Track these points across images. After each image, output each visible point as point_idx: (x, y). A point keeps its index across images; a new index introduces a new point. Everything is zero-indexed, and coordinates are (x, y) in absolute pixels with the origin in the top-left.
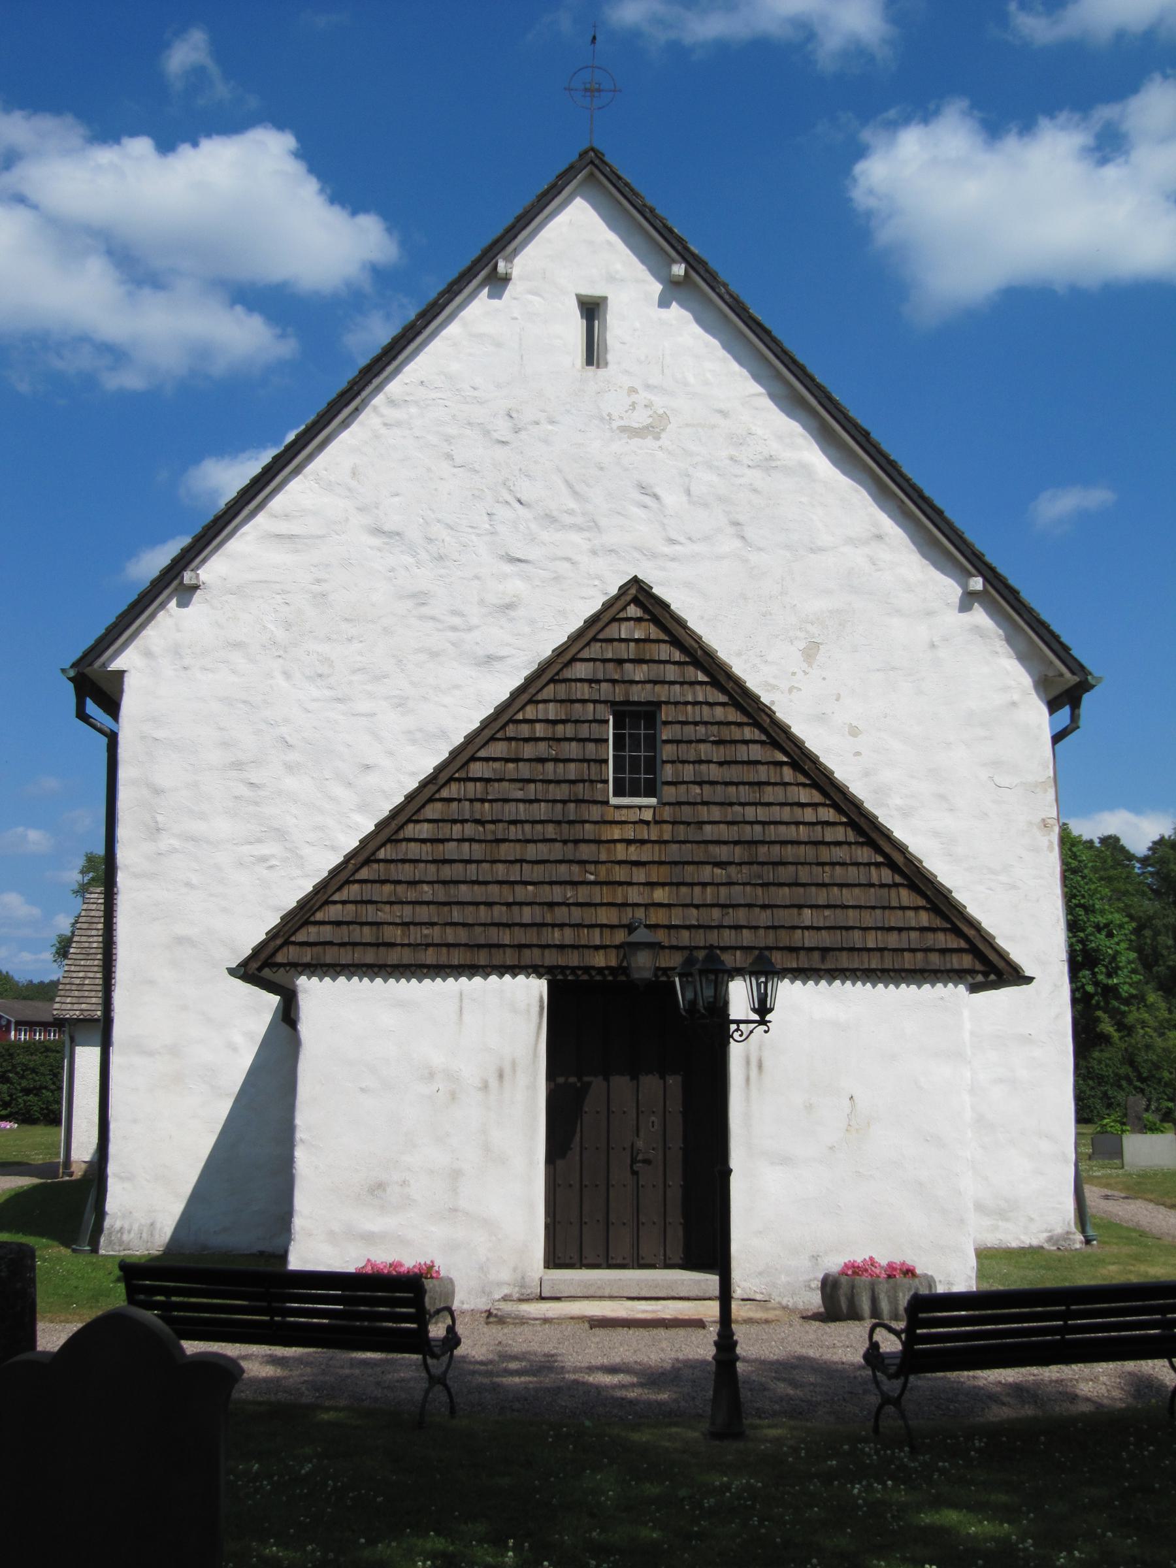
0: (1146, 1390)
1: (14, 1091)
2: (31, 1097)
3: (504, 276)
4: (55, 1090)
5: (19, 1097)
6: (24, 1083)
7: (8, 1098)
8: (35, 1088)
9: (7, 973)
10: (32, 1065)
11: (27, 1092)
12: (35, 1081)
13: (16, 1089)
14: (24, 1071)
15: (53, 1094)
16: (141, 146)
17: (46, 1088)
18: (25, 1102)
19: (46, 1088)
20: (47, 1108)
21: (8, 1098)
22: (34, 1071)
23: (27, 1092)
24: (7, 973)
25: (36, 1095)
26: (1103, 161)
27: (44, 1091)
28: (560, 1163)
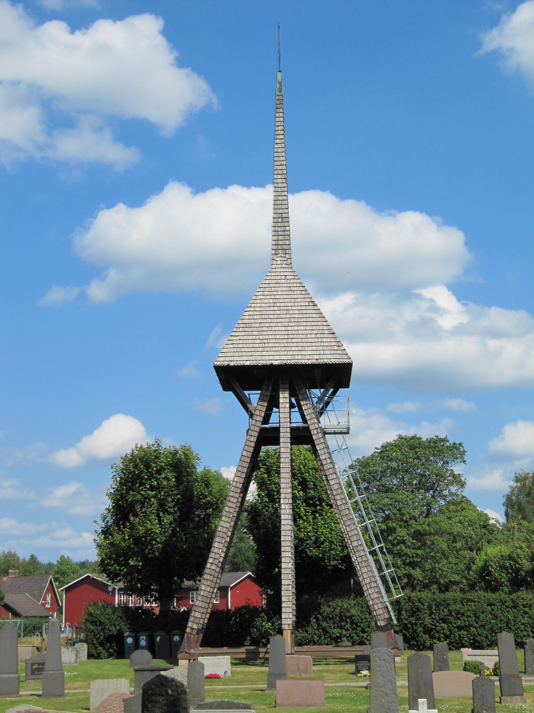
0: (336, 632)
1: (453, 628)
2: (462, 632)
3: (247, 479)
4: (478, 627)
5: (455, 632)
6: (459, 623)
7: (449, 633)
8: (465, 626)
9: (68, 557)
10: (462, 611)
11: (460, 628)
12: (465, 621)
13: (453, 627)
14: (457, 615)
15: (477, 630)
16: (121, 207)
17: (472, 626)
18: (459, 635)
19: (472, 626)
20: (474, 639)
21: (449, 633)
22: (463, 615)
23: (460, 628)
24: (68, 557)
25: (465, 630)
26: (31, 556)
27: (471, 628)
28: (67, 594)
